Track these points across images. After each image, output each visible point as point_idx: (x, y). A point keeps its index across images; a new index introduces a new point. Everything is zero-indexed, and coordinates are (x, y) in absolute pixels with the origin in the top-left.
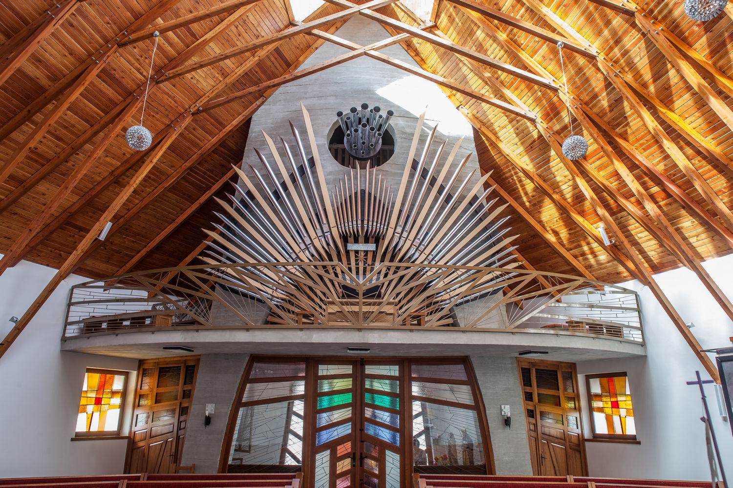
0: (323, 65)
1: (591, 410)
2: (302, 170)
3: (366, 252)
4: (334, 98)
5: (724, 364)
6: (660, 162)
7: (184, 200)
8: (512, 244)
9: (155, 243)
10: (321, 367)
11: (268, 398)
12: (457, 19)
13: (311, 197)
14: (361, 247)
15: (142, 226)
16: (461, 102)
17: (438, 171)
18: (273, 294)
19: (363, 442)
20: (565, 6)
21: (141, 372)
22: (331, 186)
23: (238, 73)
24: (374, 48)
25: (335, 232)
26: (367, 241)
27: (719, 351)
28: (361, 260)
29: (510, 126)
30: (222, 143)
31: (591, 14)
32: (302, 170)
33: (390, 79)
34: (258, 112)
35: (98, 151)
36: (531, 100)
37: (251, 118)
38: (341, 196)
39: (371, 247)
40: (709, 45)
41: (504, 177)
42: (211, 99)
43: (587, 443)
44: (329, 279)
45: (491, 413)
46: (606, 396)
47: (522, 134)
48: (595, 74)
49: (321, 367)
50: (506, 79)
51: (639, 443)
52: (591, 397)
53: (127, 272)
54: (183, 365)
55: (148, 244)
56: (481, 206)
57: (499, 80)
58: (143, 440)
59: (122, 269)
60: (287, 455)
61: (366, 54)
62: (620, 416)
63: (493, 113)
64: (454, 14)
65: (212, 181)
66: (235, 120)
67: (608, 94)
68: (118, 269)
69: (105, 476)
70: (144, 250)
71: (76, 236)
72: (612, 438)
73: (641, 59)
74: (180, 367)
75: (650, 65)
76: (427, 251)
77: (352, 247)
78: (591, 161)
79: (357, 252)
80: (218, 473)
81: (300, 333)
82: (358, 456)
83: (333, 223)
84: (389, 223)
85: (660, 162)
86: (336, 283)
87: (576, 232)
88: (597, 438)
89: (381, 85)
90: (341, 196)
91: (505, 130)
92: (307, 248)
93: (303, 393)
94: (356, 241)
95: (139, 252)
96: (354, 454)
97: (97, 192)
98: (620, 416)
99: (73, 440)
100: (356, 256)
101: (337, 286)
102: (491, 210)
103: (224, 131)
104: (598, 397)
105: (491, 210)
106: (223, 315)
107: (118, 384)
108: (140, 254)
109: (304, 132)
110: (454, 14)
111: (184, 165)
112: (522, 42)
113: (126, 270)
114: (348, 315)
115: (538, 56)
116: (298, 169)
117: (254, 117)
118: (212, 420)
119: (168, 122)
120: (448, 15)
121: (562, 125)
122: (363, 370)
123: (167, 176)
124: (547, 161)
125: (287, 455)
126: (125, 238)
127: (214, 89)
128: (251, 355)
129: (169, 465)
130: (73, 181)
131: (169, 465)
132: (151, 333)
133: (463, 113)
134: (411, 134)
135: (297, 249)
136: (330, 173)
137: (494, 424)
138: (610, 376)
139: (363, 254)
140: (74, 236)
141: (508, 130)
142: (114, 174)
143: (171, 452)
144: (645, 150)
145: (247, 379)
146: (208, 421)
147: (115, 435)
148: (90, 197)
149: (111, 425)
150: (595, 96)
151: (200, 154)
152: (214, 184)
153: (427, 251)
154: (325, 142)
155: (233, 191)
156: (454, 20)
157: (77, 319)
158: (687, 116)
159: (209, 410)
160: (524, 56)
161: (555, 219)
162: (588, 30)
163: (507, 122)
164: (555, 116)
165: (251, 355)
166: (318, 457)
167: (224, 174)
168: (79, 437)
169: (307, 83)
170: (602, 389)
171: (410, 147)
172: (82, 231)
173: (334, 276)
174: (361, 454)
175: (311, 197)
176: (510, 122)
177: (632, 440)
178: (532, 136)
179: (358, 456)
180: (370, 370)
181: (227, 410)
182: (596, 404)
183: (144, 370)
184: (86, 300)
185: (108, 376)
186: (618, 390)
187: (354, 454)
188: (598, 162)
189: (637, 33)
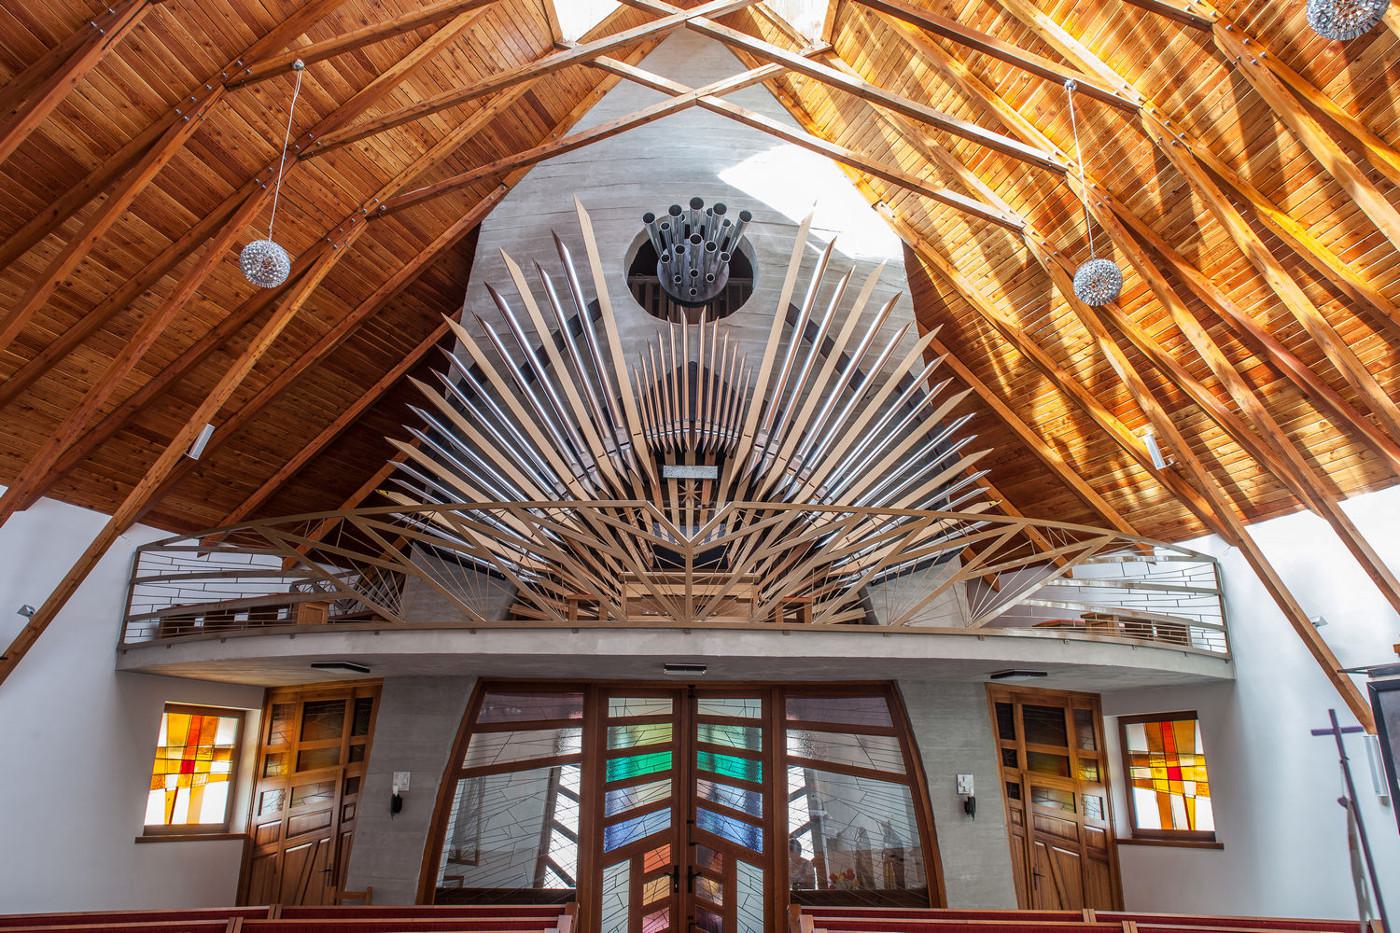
1: (1129, 784)
2: (576, 324)
3: (699, 482)
5: (1384, 697)
6: (1260, 309)
8: (979, 466)
12: (872, 37)
13: (594, 376)
14: (690, 472)
17: (836, 328)
19: (692, 844)
22: (632, 356)
23: (455, 140)
26: (700, 460)
27: (1373, 672)
28: (689, 498)
29: (973, 241)
30: (425, 274)
31: (1128, 27)
32: (576, 324)
33: (744, 151)
35: (188, 289)
36: (1014, 191)
37: (480, 225)
39: (709, 472)
40: (1355, 86)
41: (962, 338)
42: (404, 190)
43: (1121, 848)
44: (629, 534)
46: (1157, 757)
47: (997, 256)
48: (1137, 142)
50: (967, 152)
51: (1220, 847)
56: (919, 395)
62: (1184, 795)
64: (867, 27)
66: (450, 229)
67: (1160, 180)
70: (275, 478)
71: (145, 451)
72: (1168, 838)
74: (344, 701)
75: (1242, 124)
76: (816, 480)
77: (673, 472)
79: (681, 482)
81: (572, 638)
82: (683, 872)
83: (635, 427)
84: (742, 427)
85: (1260, 309)
86: (642, 542)
88: (1139, 837)
89: (728, 162)
91: (964, 248)
92: (587, 474)
93: (579, 751)
94: (680, 460)
96: (676, 868)
98: (1184, 795)
99: (138, 841)
100: (680, 490)
101: (644, 546)
102: (939, 401)
103: (428, 249)
104: (1143, 759)
105: (939, 401)
107: (225, 733)
108: (267, 485)
109: (580, 253)
112: (997, 81)
114: (665, 602)
116: (569, 322)
117: (486, 224)
118: (405, 804)
121: (1073, 239)
122: (694, 707)
123: (318, 337)
124: (1045, 307)
125: (548, 869)
127: (409, 169)
134: (786, 255)
135: (567, 476)
136: (630, 331)
138: (1166, 719)
139: (693, 486)
140: (141, 451)
143: (326, 864)
144: (1231, 286)
145: (471, 725)
146: (397, 804)
147: (220, 831)
152: (409, 352)
153: (816, 480)
154: (621, 271)
155: (445, 365)
157: (147, 610)
159: (400, 783)
160: (1001, 106)
162: (1123, 58)
163: (968, 233)
164: (1060, 221)
165: (480, 678)
166: (607, 873)
167: (427, 333)
168: (151, 836)
169: (587, 159)
171: (782, 281)
173: (637, 528)
174: (690, 868)
175: (594, 376)
176: (975, 233)
177: (1208, 841)
179: (683, 872)
182: (1139, 772)
183: (276, 707)
185: (207, 719)
187: (676, 868)
189: (1217, 63)
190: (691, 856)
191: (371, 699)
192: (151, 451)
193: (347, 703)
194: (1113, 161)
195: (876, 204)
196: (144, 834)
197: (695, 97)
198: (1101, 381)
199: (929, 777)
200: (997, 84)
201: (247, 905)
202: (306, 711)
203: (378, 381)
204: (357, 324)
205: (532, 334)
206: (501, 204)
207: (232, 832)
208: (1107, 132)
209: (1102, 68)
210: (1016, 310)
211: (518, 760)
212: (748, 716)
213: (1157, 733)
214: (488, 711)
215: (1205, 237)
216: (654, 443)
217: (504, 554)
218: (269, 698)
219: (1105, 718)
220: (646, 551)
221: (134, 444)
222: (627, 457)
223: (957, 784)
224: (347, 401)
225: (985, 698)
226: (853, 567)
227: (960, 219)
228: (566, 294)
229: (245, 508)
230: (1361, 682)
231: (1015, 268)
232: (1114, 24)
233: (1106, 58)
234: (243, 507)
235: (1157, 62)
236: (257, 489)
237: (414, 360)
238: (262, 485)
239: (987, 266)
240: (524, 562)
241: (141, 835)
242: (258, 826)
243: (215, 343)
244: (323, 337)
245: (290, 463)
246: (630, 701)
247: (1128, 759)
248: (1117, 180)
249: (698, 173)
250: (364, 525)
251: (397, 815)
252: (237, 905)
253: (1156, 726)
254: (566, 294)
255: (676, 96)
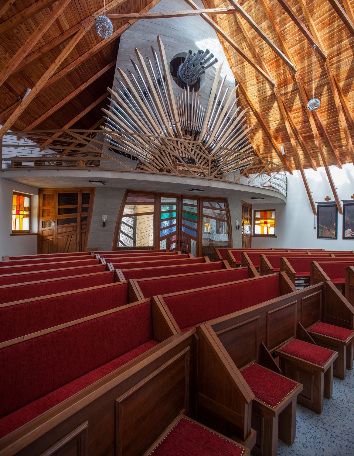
0: (179, 13)
1: (255, 224)
2: (159, 81)
4: (174, 39)
5: (320, 208)
6: (326, 120)
7: (72, 85)
9: (51, 111)
10: (162, 198)
11: (145, 212)
12: (253, 11)
15: (46, 97)
16: (233, 64)
18: (145, 155)
19: (181, 235)
20: (324, 24)
21: (42, 196)
24: (206, 12)
25: (179, 125)
27: (318, 203)
29: (256, 86)
31: (333, 34)
32: (159, 81)
33: (203, 37)
34: (125, 34)
35: (46, 27)
36: (275, 74)
37: (120, 37)
38: (180, 105)
40: (350, 67)
43: (252, 237)
44: (168, 152)
45: (233, 224)
46: (262, 219)
47: (261, 91)
48: (318, 68)
49: (162, 198)
50: (267, 58)
51: (276, 237)
52: (255, 219)
53: (33, 129)
54: (79, 192)
55: (46, 112)
57: (263, 57)
58: (51, 235)
59: (29, 126)
60: (120, 243)
61: (201, 15)
62: (267, 227)
63: (250, 76)
64: (253, 6)
65: (89, 75)
67: (319, 81)
68: (26, 126)
69: (21, 256)
70: (44, 115)
71: (7, 94)
72: (262, 235)
73: (346, 66)
74: (78, 194)
75: (349, 71)
78: (292, 113)
80: (112, 251)
81: (181, 179)
82: (179, 242)
85: (326, 120)
86: (171, 155)
87: (268, 146)
88: (255, 235)
89: (199, 40)
90: (180, 105)
91: (253, 87)
93: (176, 209)
95: (40, 116)
96: (178, 241)
97: (29, 63)
98: (267, 227)
99: (11, 235)
101: (172, 156)
104: (259, 219)
106: (109, 165)
107: (26, 202)
108: (41, 118)
110: (253, 6)
111: (79, 59)
112: (288, 38)
113: (32, 127)
115: (292, 49)
118: (106, 224)
119: (79, 21)
120: (249, 5)
121: (286, 91)
122: (182, 201)
123: (67, 64)
124: (270, 109)
125: (120, 243)
126: (35, 104)
128: (127, 189)
129: (76, 248)
130: (29, 48)
131: (76, 248)
132: (56, 170)
133: (233, 71)
137: (233, 228)
138: (265, 211)
140: (5, 94)
141: (255, 87)
142: (42, 50)
143: (76, 241)
144: (321, 113)
145: (124, 203)
146: (104, 224)
147: (28, 233)
148: (24, 65)
149: (26, 228)
150: (311, 81)
151: (90, 53)
156: (251, 10)
157: (8, 157)
158: (350, 101)
159: (105, 218)
160: (286, 46)
161: (261, 139)
162: (327, 43)
163: (255, 83)
164: (284, 86)
165: (127, 189)
166: (161, 242)
168: (15, 233)
169: (157, 23)
170: (261, 216)
172: (11, 91)
173: (170, 150)
174: (181, 241)
176: (258, 83)
177: (273, 236)
178: (266, 94)
179: (179, 242)
180: (185, 201)
181: (115, 219)
182: (257, 222)
183: (44, 195)
184: (19, 144)
185: (21, 197)
186: (268, 217)
187: (178, 241)
188: (296, 114)
189: (352, 52)
190: (181, 238)
191: (90, 193)
192: (8, 95)
193: (78, 194)
194: (308, 72)
195: (231, 67)
196: (12, 233)
197: (201, 12)
198: (276, 131)
199: (232, 221)
200: (287, 39)
201: (57, 253)
202: (59, 196)
203: (79, 87)
204: (81, 63)
205: (147, 82)
206: (127, 31)
207: (31, 233)
208: (311, 63)
209: (321, 43)
210: (260, 108)
211: (147, 212)
212: (194, 204)
213: (263, 214)
214: (129, 199)
215: (322, 99)
216: (186, 126)
217: (142, 153)
218: (40, 191)
219: (252, 210)
220: (172, 157)
221: (4, 90)
222: (174, 128)
223: (236, 222)
224: (69, 92)
225: (241, 204)
226: (227, 168)
227: (255, 78)
228: (157, 72)
229: (34, 125)
230: (316, 205)
231: (265, 96)
232: (329, 32)
233: (323, 41)
234: (33, 124)
235: (335, 47)
236: (37, 119)
237: (92, 82)
238: (39, 117)
239: (257, 94)
240: (148, 156)
241: (12, 233)
242: (42, 231)
243: (40, 55)
244: (69, 65)
245: (49, 111)
246: (166, 198)
247: (255, 219)
248: (306, 78)
249: (191, 41)
250: (77, 136)
251: (105, 227)
252: (38, 254)
253: (263, 212)
254: (157, 72)
255: (194, 9)
